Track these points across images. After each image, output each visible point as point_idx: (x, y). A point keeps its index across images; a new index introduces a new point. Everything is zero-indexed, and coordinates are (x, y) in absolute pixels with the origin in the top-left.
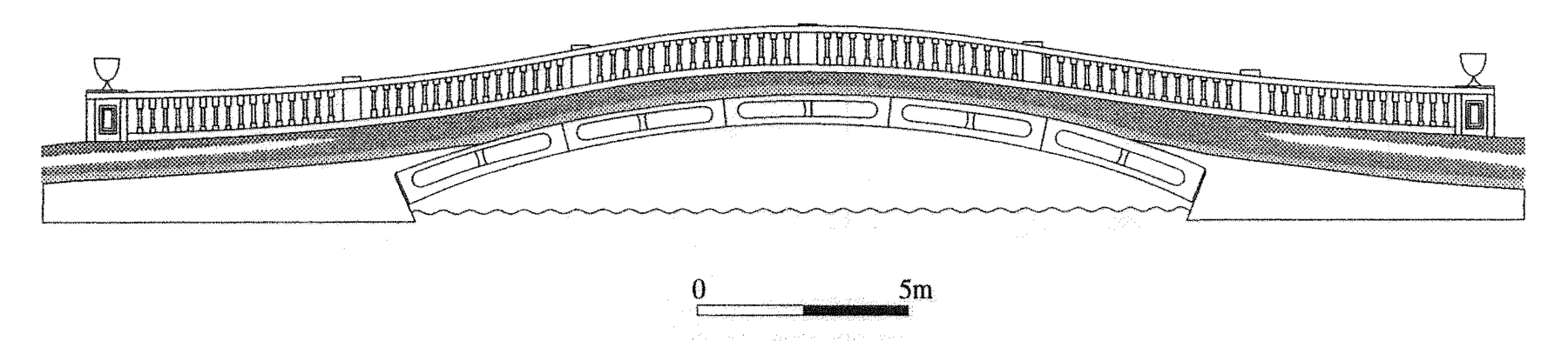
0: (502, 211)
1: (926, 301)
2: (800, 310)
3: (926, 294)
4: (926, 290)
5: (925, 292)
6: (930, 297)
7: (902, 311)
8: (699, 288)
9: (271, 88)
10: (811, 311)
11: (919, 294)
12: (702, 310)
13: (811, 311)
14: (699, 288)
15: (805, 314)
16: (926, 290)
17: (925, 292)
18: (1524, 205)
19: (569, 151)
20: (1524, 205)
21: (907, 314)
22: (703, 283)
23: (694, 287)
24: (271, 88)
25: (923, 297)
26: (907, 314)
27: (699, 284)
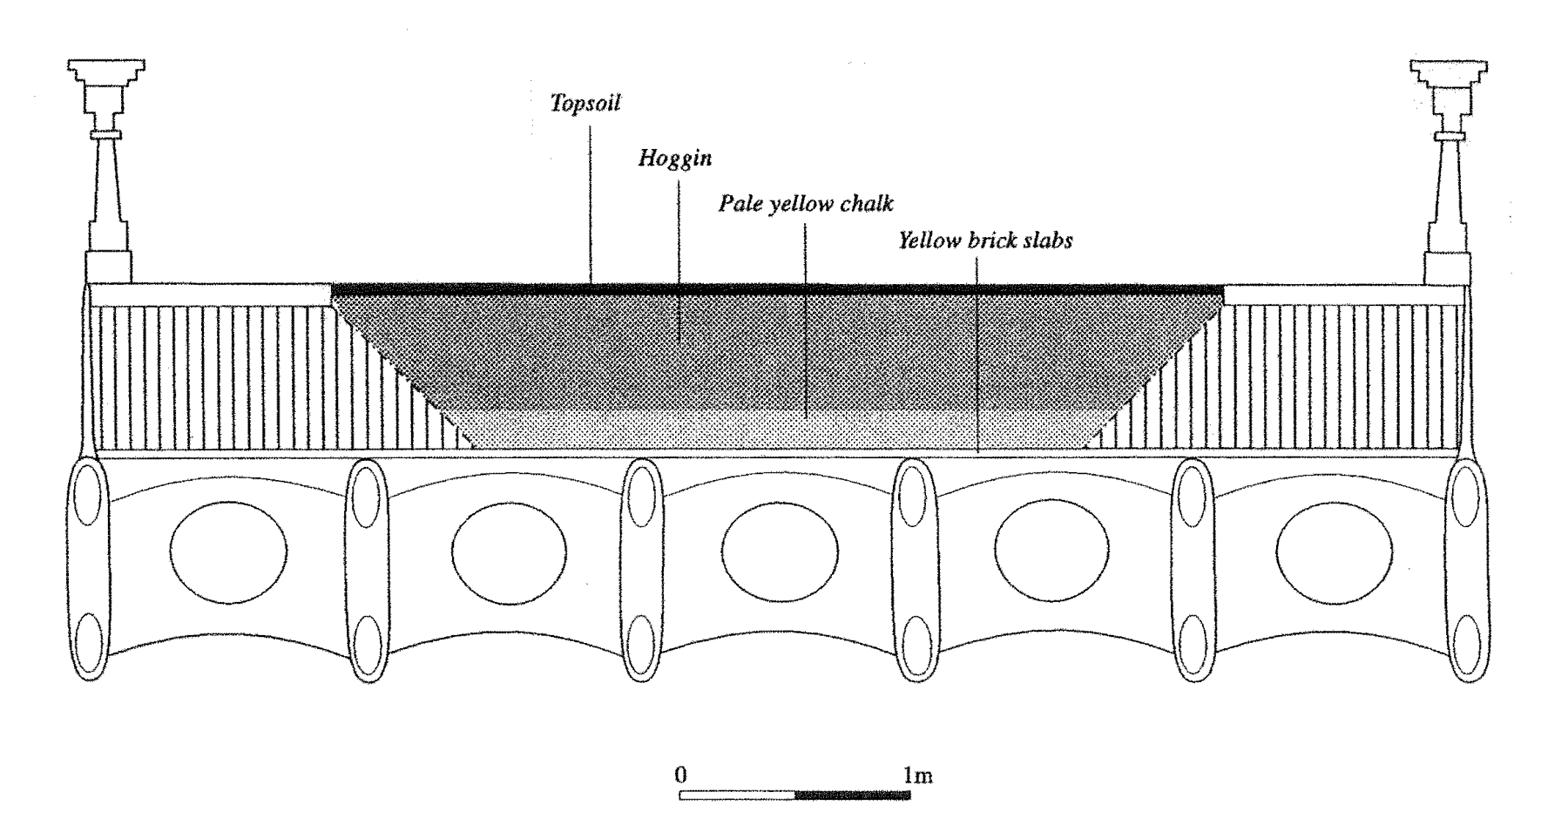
0: (1108, 541)
1: (928, 784)
2: (792, 795)
3: (927, 779)
4: (927, 775)
5: (924, 777)
6: (931, 781)
7: (906, 796)
8: (681, 774)
9: (101, 331)
10: (802, 796)
11: (921, 779)
12: (684, 795)
13: (802, 796)
14: (681, 774)
15: (796, 798)
16: (927, 775)
17: (924, 777)
18: (591, 244)
19: (1425, 285)
20: (591, 244)
21: (909, 798)
22: (685, 771)
23: (677, 774)
24: (101, 331)
25: (924, 782)
26: (909, 798)
27: (681, 771)
